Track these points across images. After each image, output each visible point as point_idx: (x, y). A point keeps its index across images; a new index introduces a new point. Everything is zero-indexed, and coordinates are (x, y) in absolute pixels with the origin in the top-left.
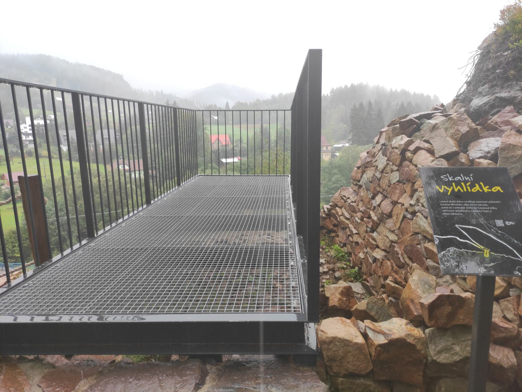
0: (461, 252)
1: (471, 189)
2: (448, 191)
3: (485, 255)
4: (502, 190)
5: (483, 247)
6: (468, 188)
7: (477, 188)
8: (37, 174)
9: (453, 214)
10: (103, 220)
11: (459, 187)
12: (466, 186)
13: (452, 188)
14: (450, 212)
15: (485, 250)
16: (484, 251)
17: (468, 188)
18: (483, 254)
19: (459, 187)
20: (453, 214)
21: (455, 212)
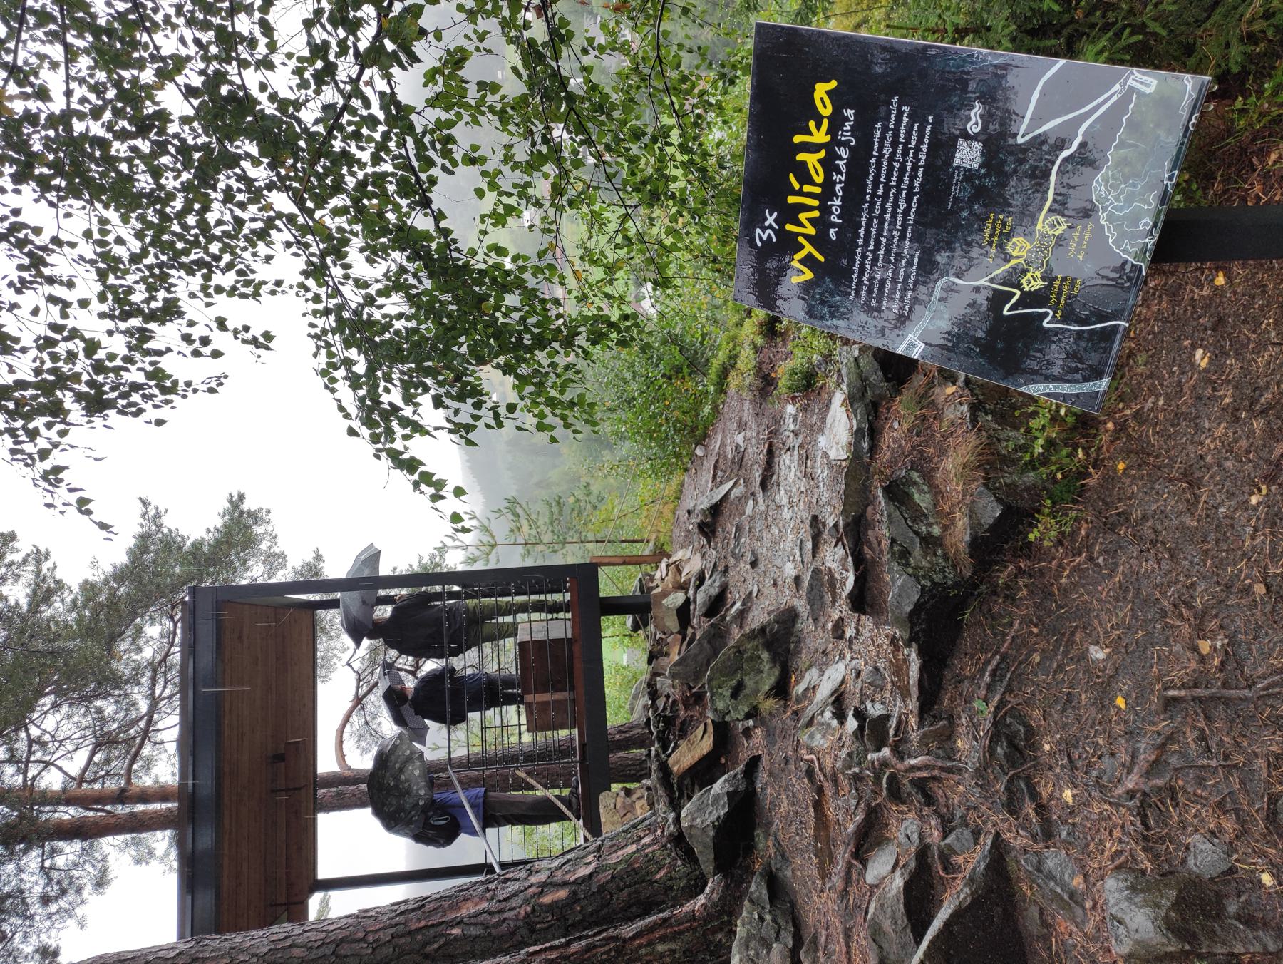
0: (1117, 164)
1: (813, 183)
2: (810, 254)
3: (1148, 90)
4: (828, 81)
5: (1117, 87)
6: (807, 188)
7: (811, 160)
8: (323, 873)
9: (922, 156)
10: (137, 753)
11: (803, 217)
12: (800, 193)
13: (801, 239)
14: (915, 168)
15: (1131, 82)
16: (1132, 89)
17: (807, 188)
18: (1141, 94)
19: (803, 217)
20: (922, 156)
21: (918, 150)
